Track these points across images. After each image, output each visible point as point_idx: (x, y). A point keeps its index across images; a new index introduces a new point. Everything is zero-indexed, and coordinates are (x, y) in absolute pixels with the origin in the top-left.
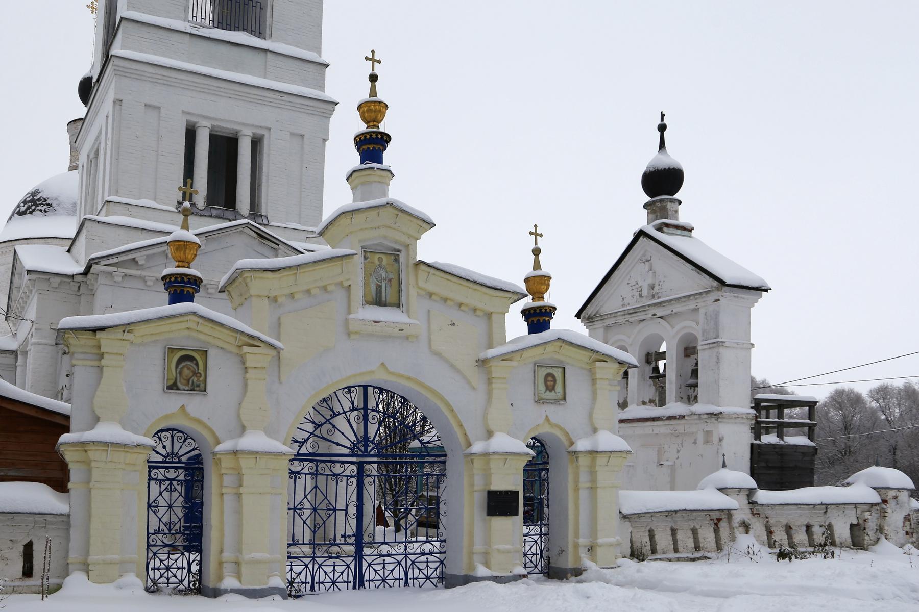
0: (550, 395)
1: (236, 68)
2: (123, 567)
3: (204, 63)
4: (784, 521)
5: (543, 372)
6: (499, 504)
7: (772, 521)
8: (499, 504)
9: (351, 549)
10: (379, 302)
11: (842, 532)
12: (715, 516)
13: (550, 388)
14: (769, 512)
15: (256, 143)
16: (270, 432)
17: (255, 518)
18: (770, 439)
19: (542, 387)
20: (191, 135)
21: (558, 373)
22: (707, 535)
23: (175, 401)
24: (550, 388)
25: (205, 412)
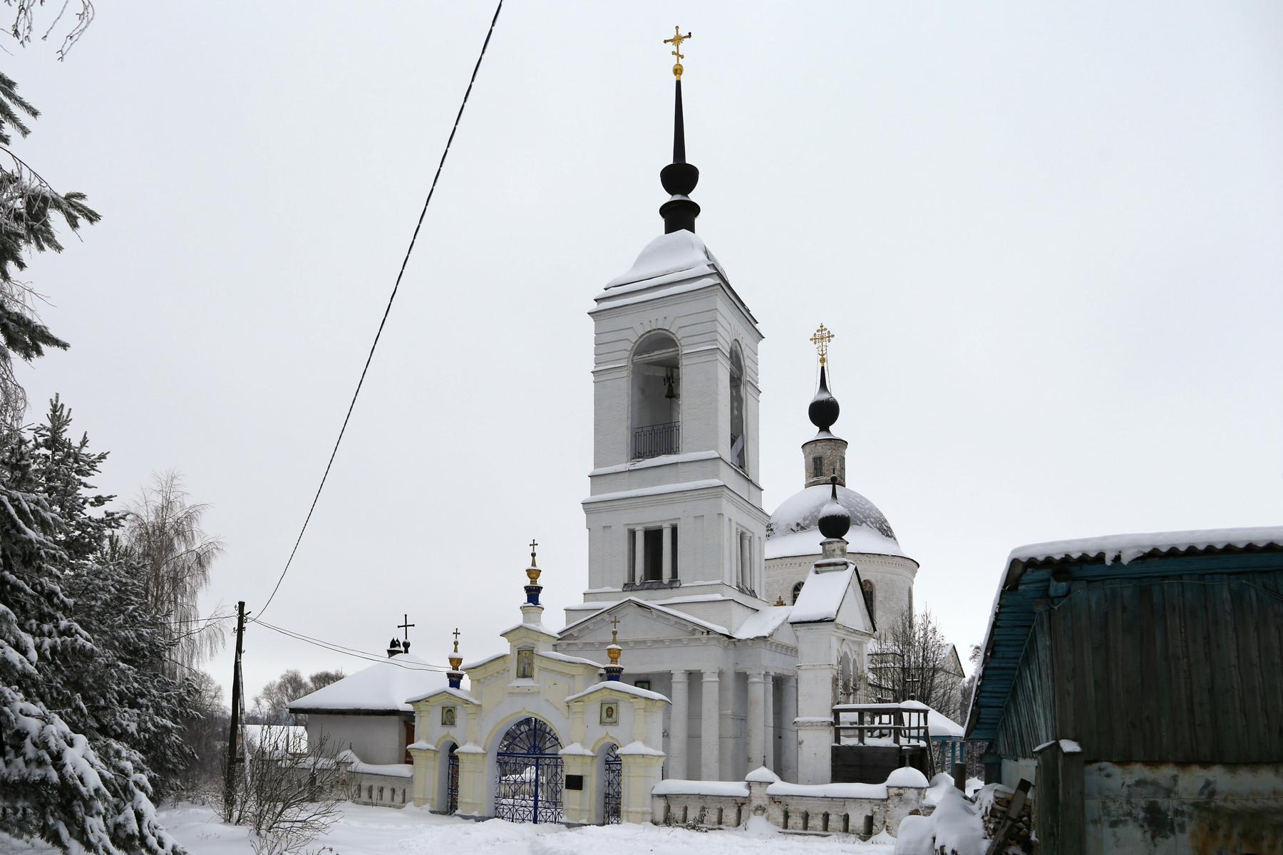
0: (609, 720)
1: (659, 483)
2: (425, 800)
3: (640, 486)
4: (803, 809)
5: (605, 707)
6: (575, 783)
7: (791, 808)
8: (575, 783)
9: (532, 803)
10: (524, 676)
11: (857, 821)
12: (740, 801)
13: (609, 716)
14: (788, 800)
15: (674, 530)
16: (476, 742)
17: (477, 781)
18: (850, 741)
19: (604, 715)
20: (633, 534)
21: (613, 707)
22: (730, 815)
23: (446, 730)
24: (609, 716)
25: (454, 733)
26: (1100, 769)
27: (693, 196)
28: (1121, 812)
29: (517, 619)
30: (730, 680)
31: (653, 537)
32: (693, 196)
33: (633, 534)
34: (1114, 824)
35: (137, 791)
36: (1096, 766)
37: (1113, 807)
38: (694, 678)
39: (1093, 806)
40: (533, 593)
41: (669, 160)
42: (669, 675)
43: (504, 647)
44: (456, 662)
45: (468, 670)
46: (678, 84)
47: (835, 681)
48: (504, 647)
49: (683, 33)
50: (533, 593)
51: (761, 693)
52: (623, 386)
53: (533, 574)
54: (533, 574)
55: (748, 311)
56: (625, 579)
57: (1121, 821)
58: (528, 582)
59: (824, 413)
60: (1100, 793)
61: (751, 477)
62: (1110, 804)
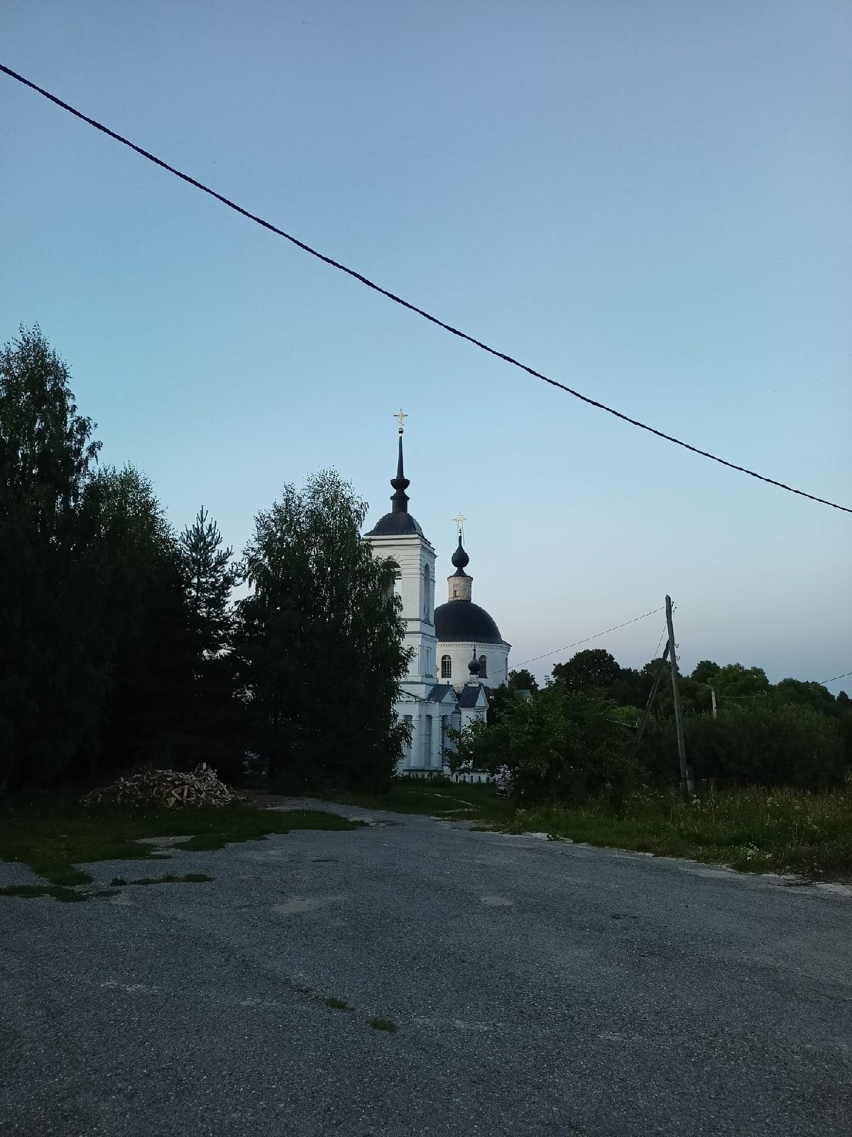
30: (424, 718)
32: (407, 492)
41: (394, 475)
59: (461, 559)
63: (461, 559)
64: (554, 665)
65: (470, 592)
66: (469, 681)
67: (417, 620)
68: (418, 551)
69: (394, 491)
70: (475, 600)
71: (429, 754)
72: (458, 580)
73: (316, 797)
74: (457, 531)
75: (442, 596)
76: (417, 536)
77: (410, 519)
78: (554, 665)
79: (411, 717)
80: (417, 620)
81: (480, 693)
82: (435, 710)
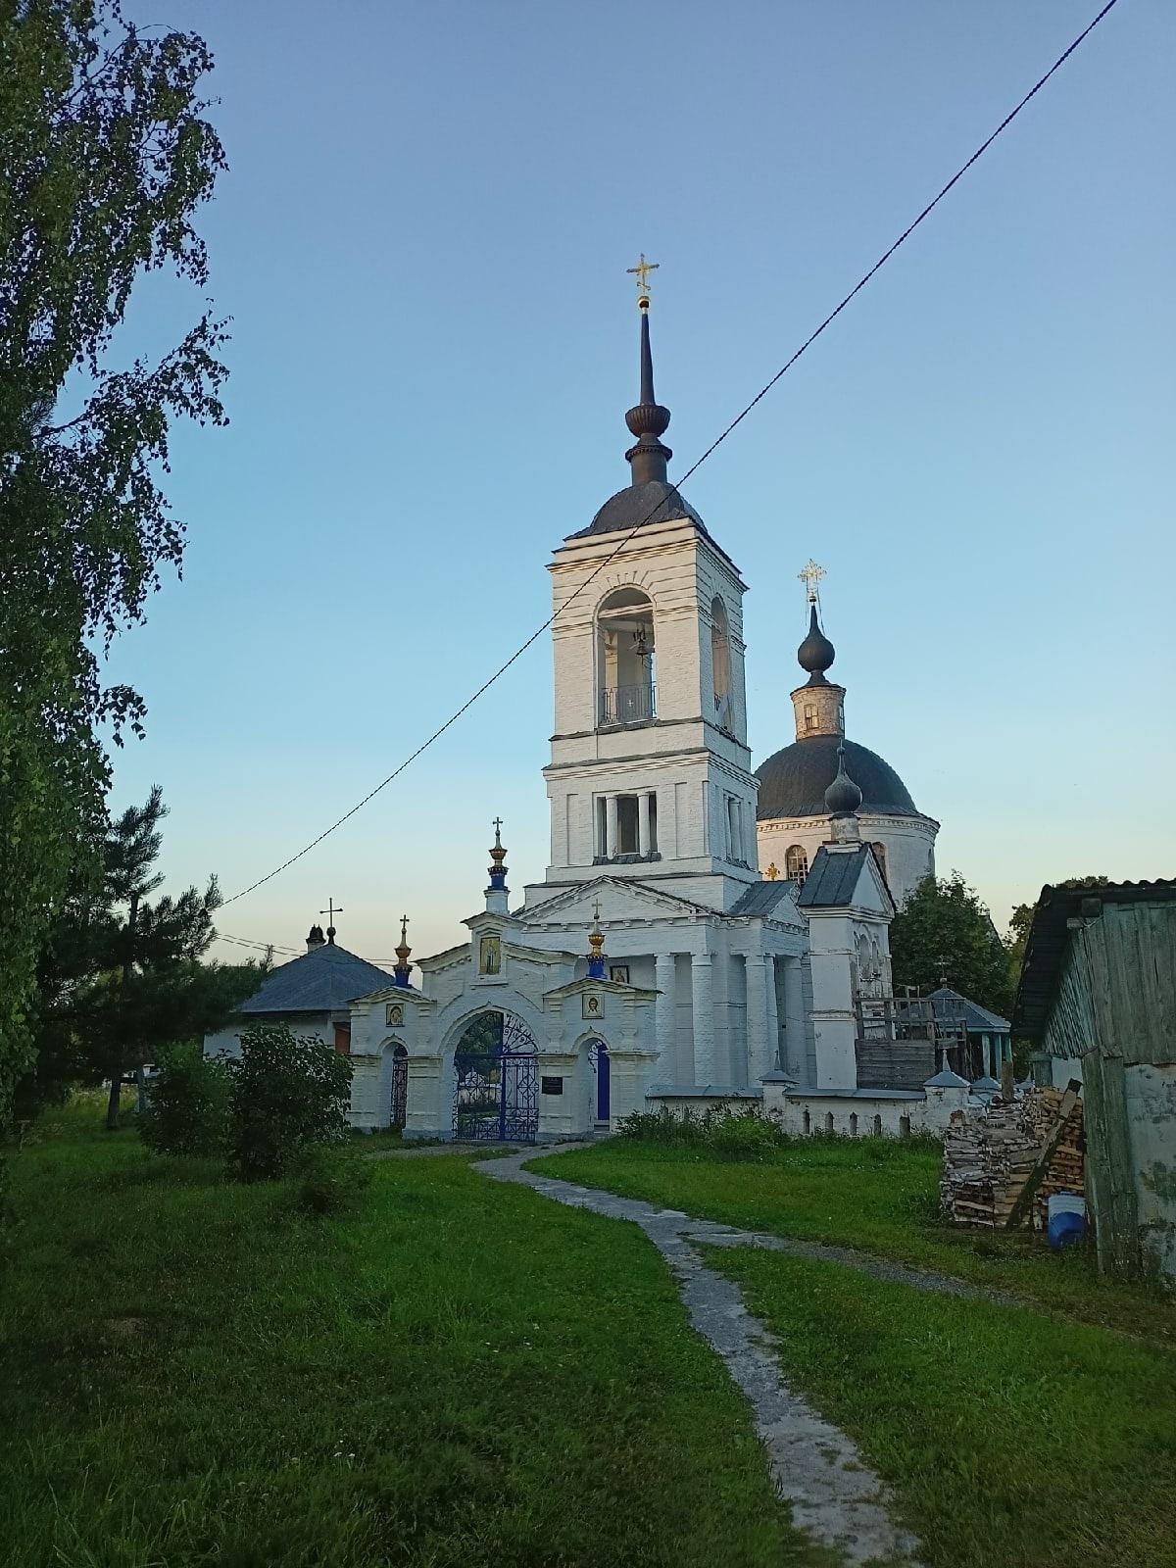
15: (652, 797)
26: (1141, 1071)
27: (664, 439)
28: (1164, 1110)
29: (480, 906)
30: (724, 961)
31: (627, 805)
32: (664, 439)
33: (603, 801)
34: (1157, 1120)
35: (158, 1159)
36: (1136, 1068)
37: (1155, 1104)
38: (682, 959)
39: (1136, 1105)
40: (498, 873)
41: (636, 400)
42: (651, 959)
43: (466, 936)
44: (403, 951)
45: (419, 962)
46: (645, 318)
47: (853, 967)
48: (466, 936)
49: (649, 262)
50: (498, 873)
51: (759, 973)
52: (585, 645)
53: (498, 853)
54: (498, 853)
55: (729, 560)
56: (593, 850)
57: (1164, 1118)
58: (492, 863)
59: (817, 655)
60: (1142, 1093)
61: (736, 733)
62: (1152, 1102)
63: (817, 655)
64: (1014, 908)
65: (841, 719)
66: (829, 838)
67: (696, 721)
68: (690, 555)
69: (633, 441)
70: (855, 733)
71: (741, 1054)
72: (816, 697)
73: (647, 1200)
74: (805, 597)
75: (772, 727)
76: (686, 521)
77: (673, 491)
78: (1014, 908)
79: (688, 956)
80: (696, 721)
81: (865, 865)
82: (752, 936)
